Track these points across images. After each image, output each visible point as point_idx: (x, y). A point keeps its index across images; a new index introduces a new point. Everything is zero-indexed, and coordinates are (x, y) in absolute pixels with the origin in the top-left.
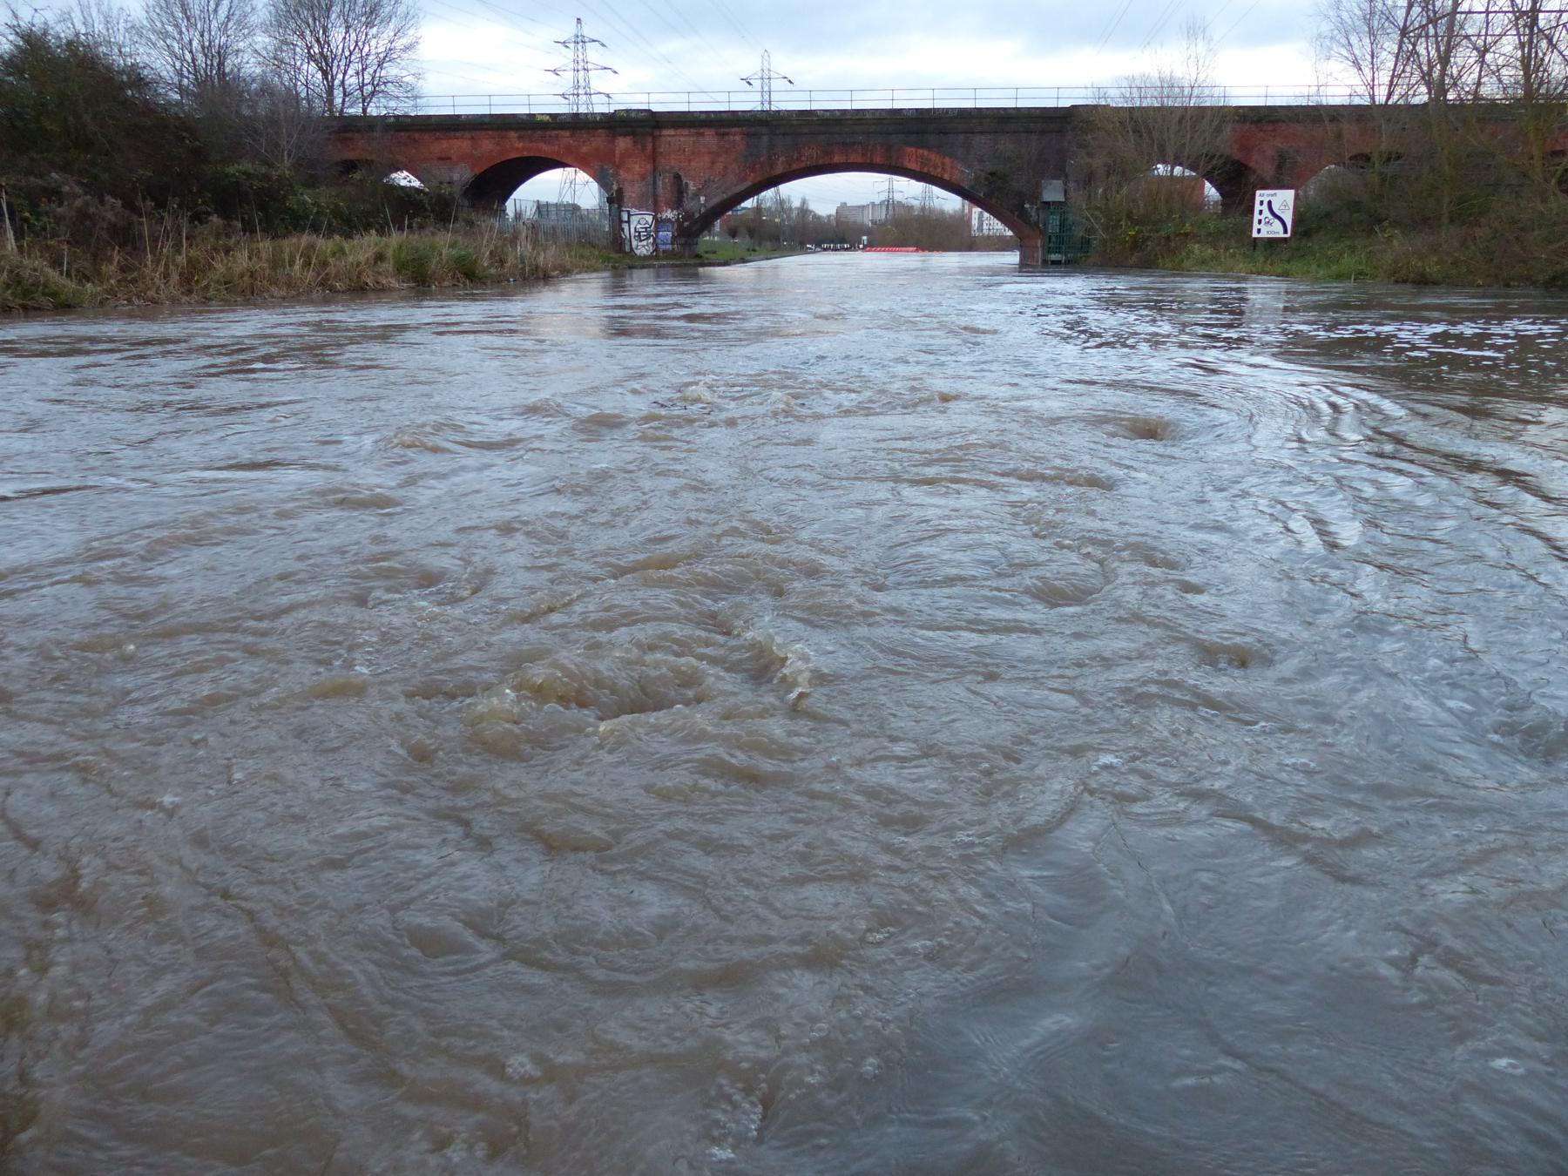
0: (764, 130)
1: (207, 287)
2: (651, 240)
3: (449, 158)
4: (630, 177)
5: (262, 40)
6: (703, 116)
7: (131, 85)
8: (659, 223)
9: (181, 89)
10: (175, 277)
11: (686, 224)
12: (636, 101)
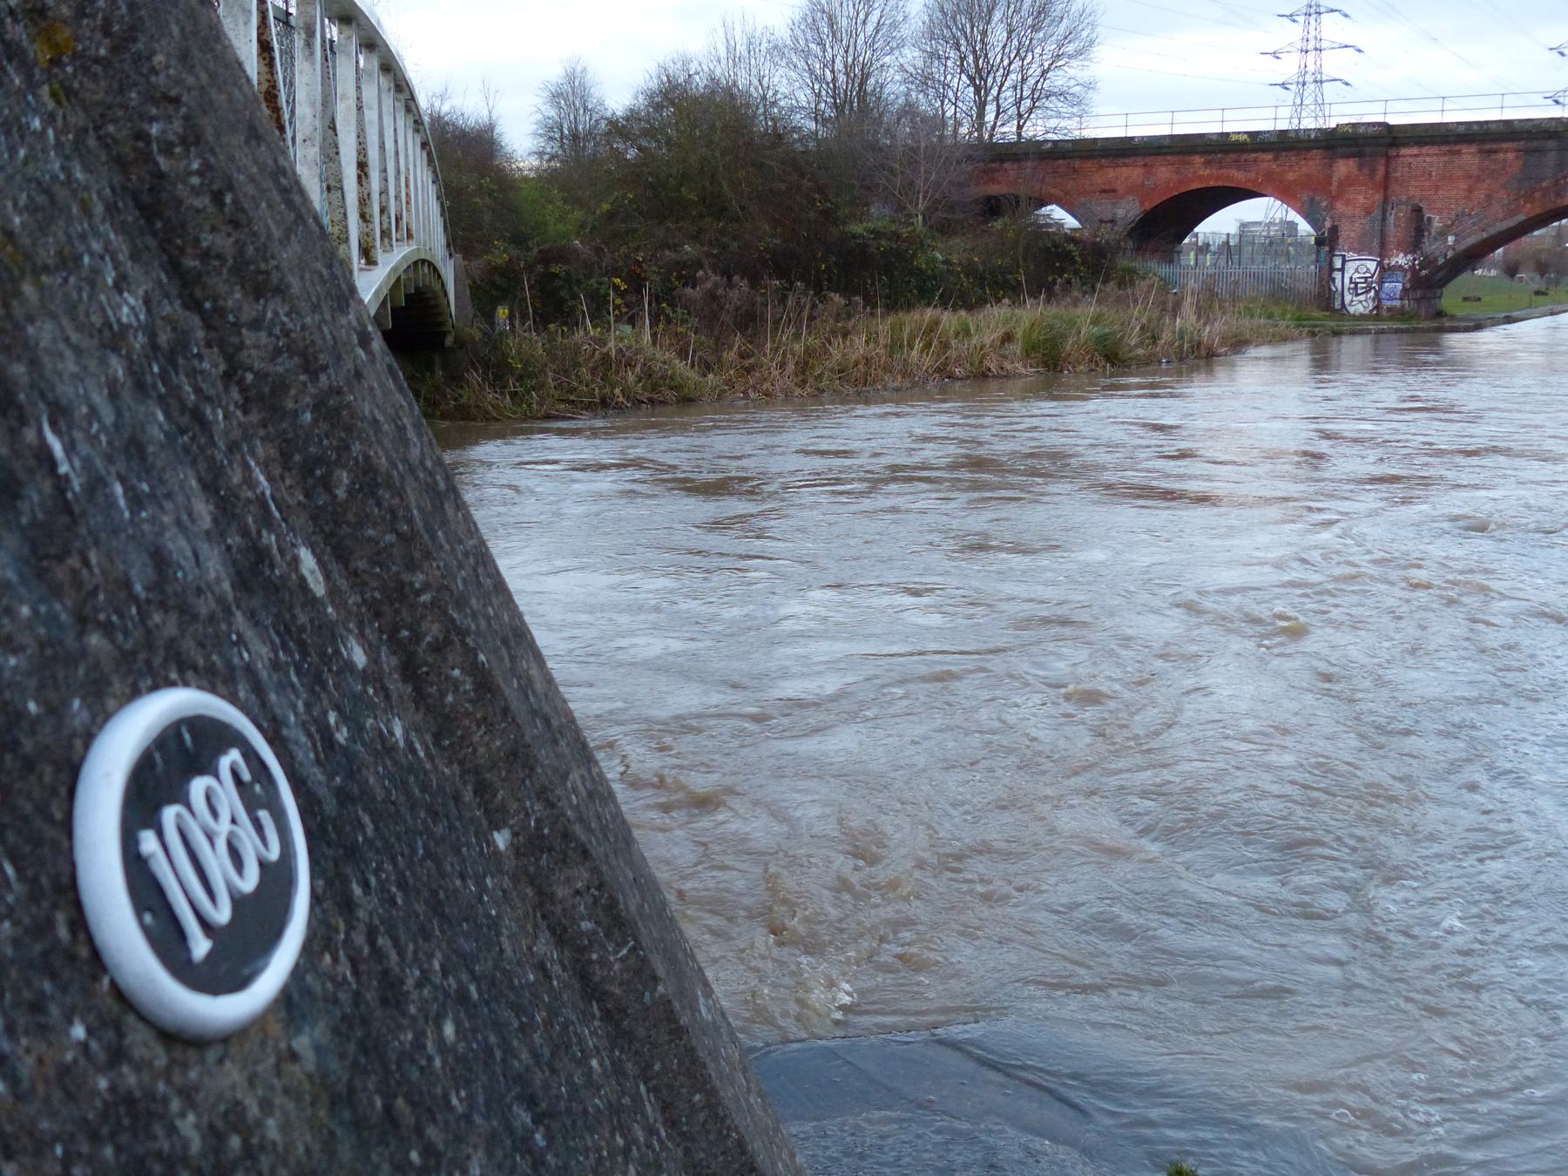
0: (1551, 144)
1: (821, 376)
2: (1372, 293)
3: (1114, 191)
4: (1349, 211)
5: (911, 56)
6: (1462, 129)
7: (773, 146)
8: (1385, 271)
9: (817, 116)
10: (791, 367)
11: (1424, 272)
12: (1371, 114)
